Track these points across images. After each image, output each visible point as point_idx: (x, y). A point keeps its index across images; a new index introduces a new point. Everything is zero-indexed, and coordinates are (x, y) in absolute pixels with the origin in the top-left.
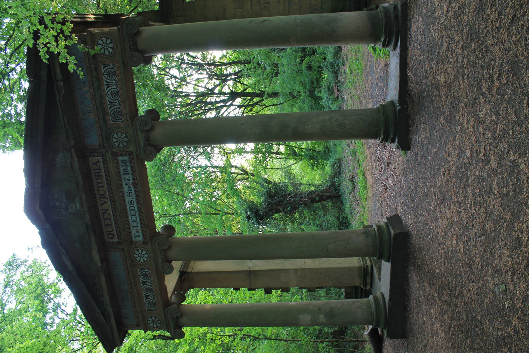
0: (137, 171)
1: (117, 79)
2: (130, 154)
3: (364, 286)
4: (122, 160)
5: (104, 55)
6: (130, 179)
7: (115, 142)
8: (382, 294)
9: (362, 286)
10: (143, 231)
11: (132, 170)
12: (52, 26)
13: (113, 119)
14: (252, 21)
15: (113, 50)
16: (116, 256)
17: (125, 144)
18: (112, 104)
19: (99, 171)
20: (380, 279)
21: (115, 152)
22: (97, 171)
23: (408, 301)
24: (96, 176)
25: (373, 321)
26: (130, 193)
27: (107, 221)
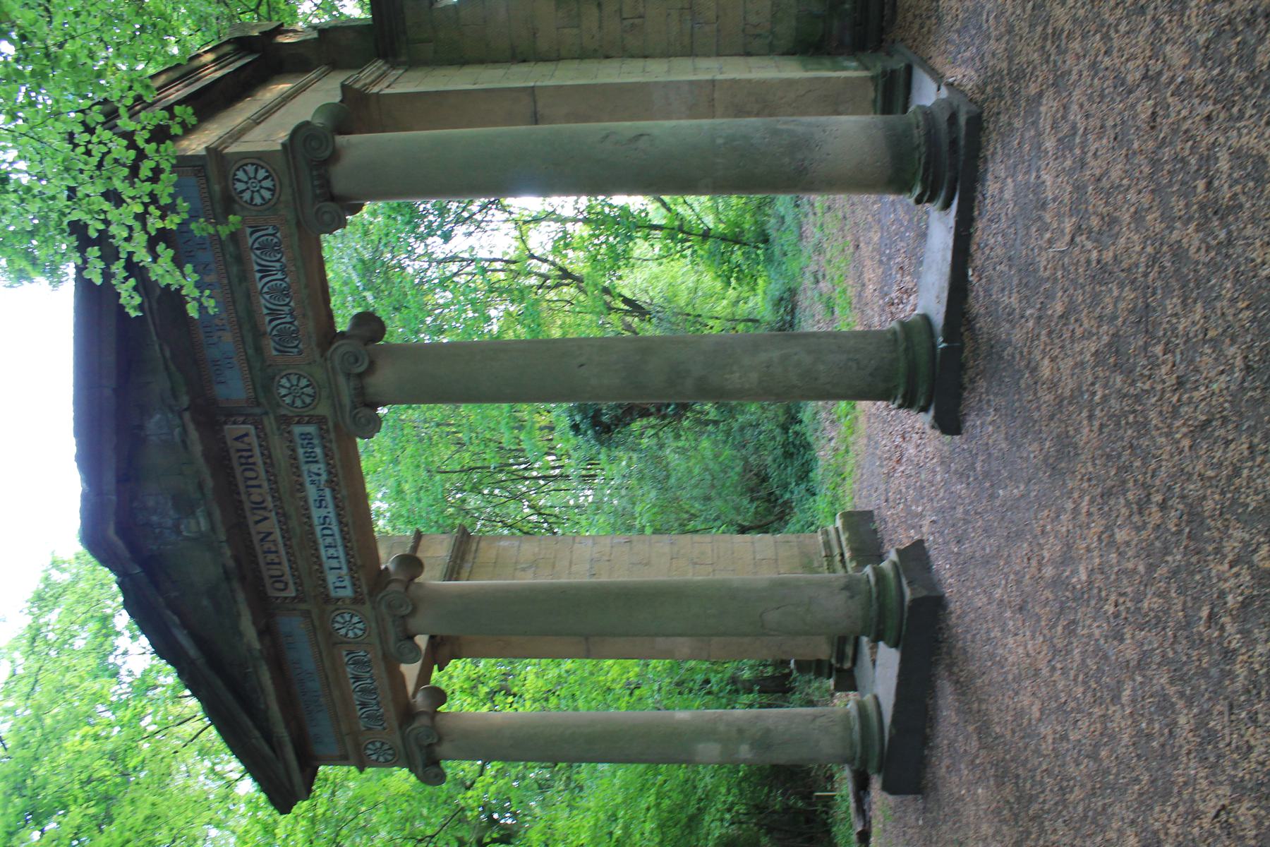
0: (337, 457)
1: (283, 260)
2: (320, 421)
3: (838, 662)
4: (302, 434)
5: (251, 204)
6: (321, 472)
7: (285, 396)
8: (876, 698)
9: (833, 661)
10: (352, 577)
11: (326, 455)
12: (132, 193)
13: (278, 347)
14: (607, 136)
15: (273, 195)
16: (293, 626)
17: (308, 400)
18: (274, 314)
19: (249, 454)
20: (874, 662)
21: (284, 415)
22: (245, 454)
23: (931, 727)
24: (242, 464)
25: (854, 759)
26: (320, 503)
27: (271, 557)
